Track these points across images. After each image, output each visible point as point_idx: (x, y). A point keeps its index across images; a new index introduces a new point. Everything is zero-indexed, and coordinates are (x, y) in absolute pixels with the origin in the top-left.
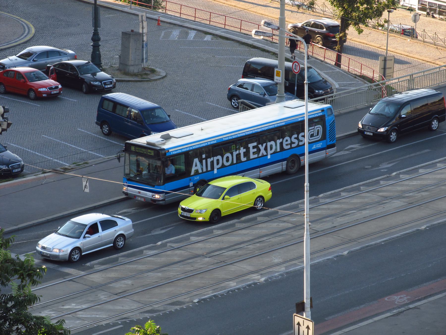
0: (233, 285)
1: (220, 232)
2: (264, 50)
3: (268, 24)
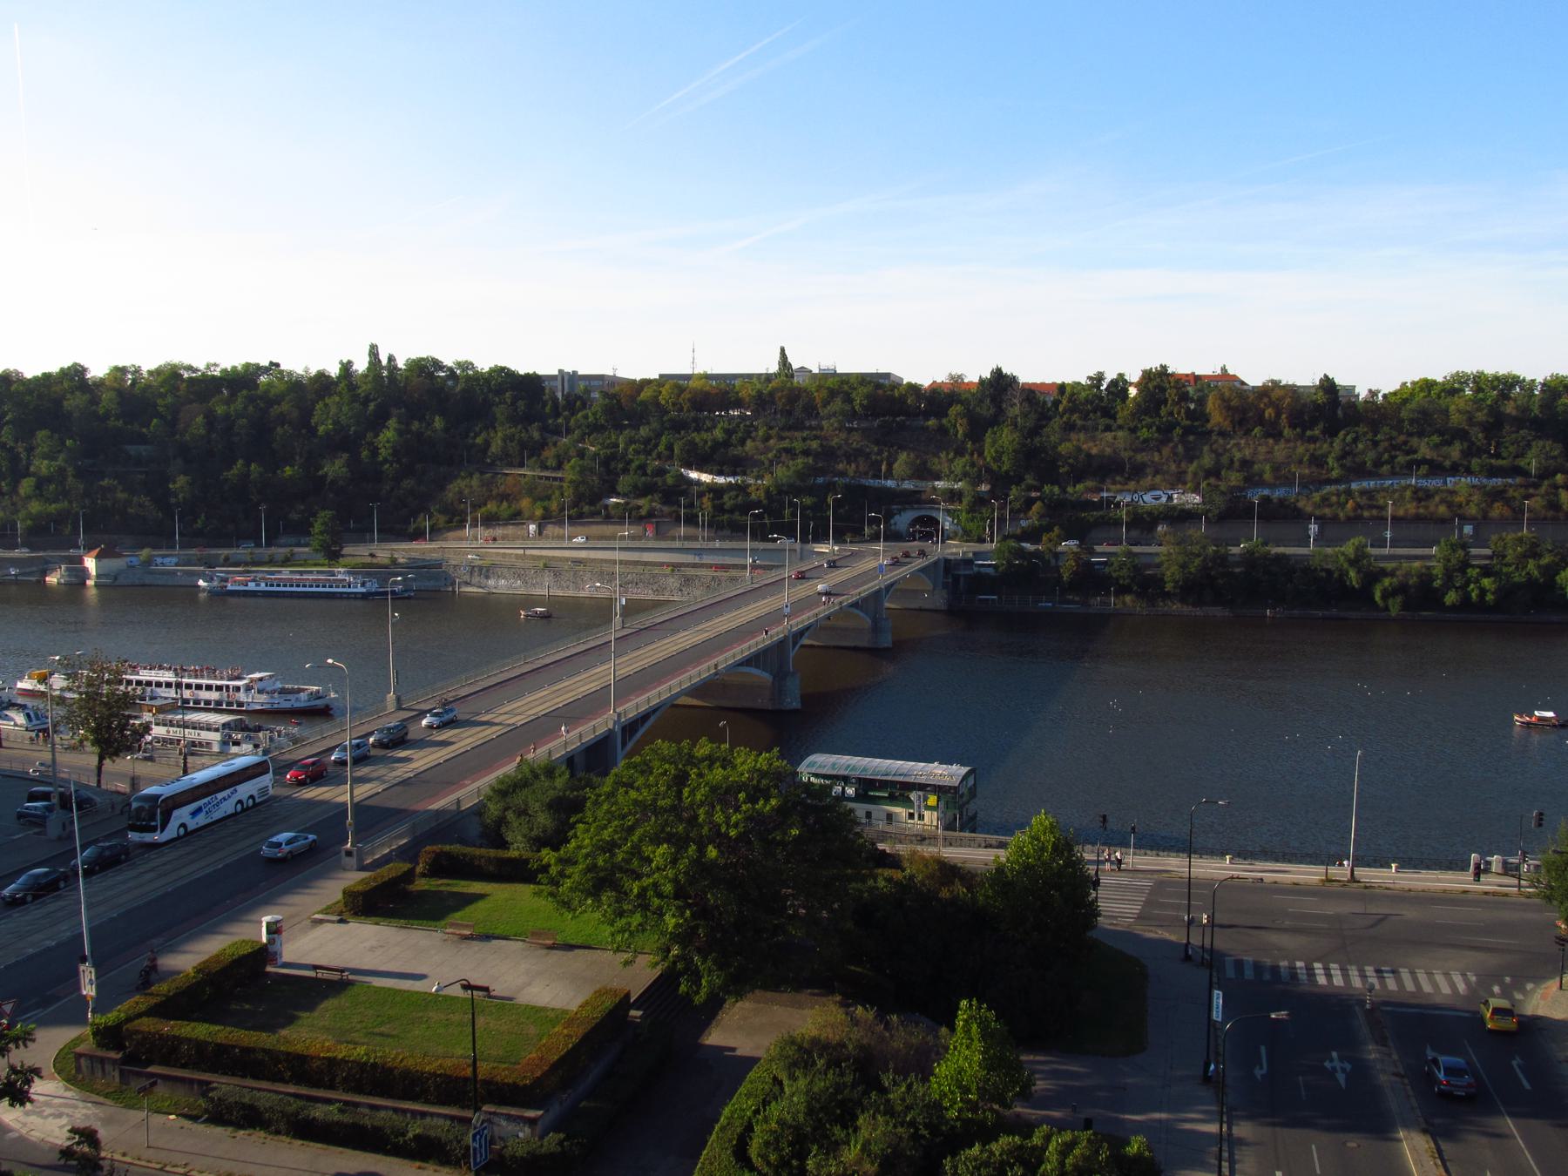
0: (31, 951)
1: (18, 915)
2: (42, 782)
3: (41, 764)
